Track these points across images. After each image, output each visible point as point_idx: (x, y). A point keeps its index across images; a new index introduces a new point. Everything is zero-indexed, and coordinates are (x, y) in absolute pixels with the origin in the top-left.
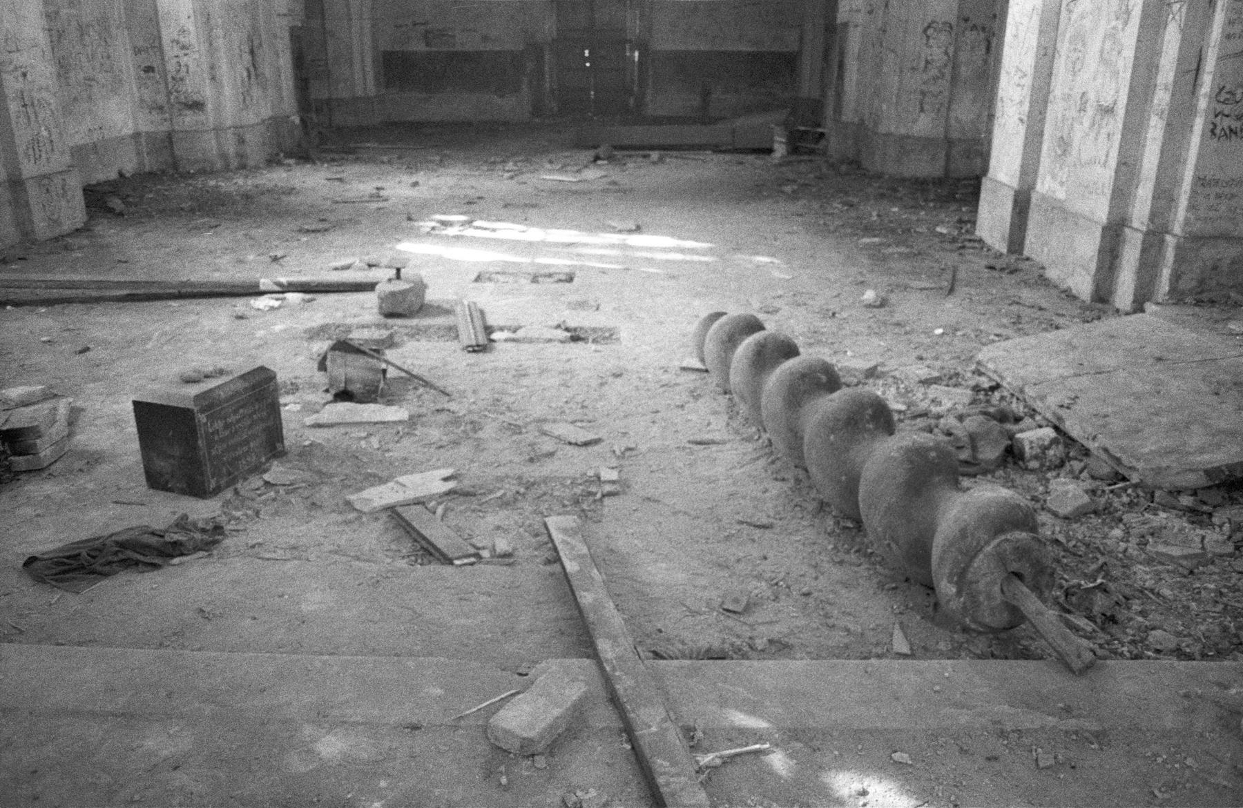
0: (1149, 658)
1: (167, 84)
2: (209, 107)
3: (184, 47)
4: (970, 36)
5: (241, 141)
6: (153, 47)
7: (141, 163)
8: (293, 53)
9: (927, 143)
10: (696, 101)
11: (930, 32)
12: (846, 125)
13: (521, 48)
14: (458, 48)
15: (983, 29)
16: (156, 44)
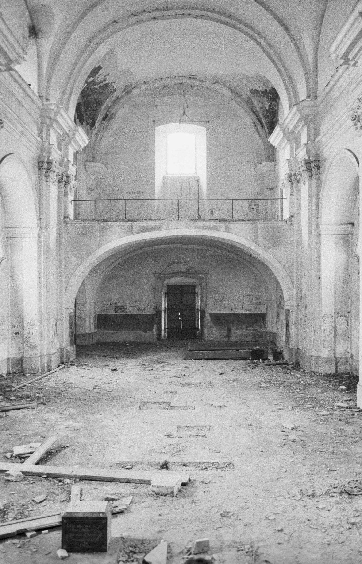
0: (84, 85)
1: (23, 339)
2: (39, 347)
3: (32, 325)
4: (340, 319)
5: (50, 360)
6: (19, 325)
7: (9, 370)
8: (70, 323)
9: (328, 360)
10: (225, 333)
11: (324, 318)
12: (291, 349)
13: (154, 313)
14: (128, 313)
15: (345, 316)
16: (21, 324)
